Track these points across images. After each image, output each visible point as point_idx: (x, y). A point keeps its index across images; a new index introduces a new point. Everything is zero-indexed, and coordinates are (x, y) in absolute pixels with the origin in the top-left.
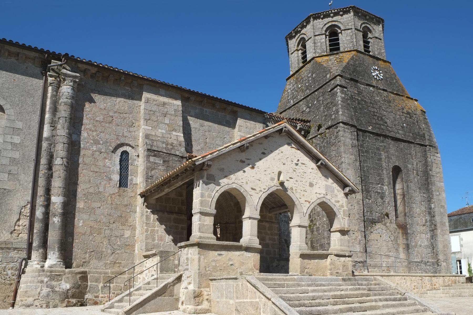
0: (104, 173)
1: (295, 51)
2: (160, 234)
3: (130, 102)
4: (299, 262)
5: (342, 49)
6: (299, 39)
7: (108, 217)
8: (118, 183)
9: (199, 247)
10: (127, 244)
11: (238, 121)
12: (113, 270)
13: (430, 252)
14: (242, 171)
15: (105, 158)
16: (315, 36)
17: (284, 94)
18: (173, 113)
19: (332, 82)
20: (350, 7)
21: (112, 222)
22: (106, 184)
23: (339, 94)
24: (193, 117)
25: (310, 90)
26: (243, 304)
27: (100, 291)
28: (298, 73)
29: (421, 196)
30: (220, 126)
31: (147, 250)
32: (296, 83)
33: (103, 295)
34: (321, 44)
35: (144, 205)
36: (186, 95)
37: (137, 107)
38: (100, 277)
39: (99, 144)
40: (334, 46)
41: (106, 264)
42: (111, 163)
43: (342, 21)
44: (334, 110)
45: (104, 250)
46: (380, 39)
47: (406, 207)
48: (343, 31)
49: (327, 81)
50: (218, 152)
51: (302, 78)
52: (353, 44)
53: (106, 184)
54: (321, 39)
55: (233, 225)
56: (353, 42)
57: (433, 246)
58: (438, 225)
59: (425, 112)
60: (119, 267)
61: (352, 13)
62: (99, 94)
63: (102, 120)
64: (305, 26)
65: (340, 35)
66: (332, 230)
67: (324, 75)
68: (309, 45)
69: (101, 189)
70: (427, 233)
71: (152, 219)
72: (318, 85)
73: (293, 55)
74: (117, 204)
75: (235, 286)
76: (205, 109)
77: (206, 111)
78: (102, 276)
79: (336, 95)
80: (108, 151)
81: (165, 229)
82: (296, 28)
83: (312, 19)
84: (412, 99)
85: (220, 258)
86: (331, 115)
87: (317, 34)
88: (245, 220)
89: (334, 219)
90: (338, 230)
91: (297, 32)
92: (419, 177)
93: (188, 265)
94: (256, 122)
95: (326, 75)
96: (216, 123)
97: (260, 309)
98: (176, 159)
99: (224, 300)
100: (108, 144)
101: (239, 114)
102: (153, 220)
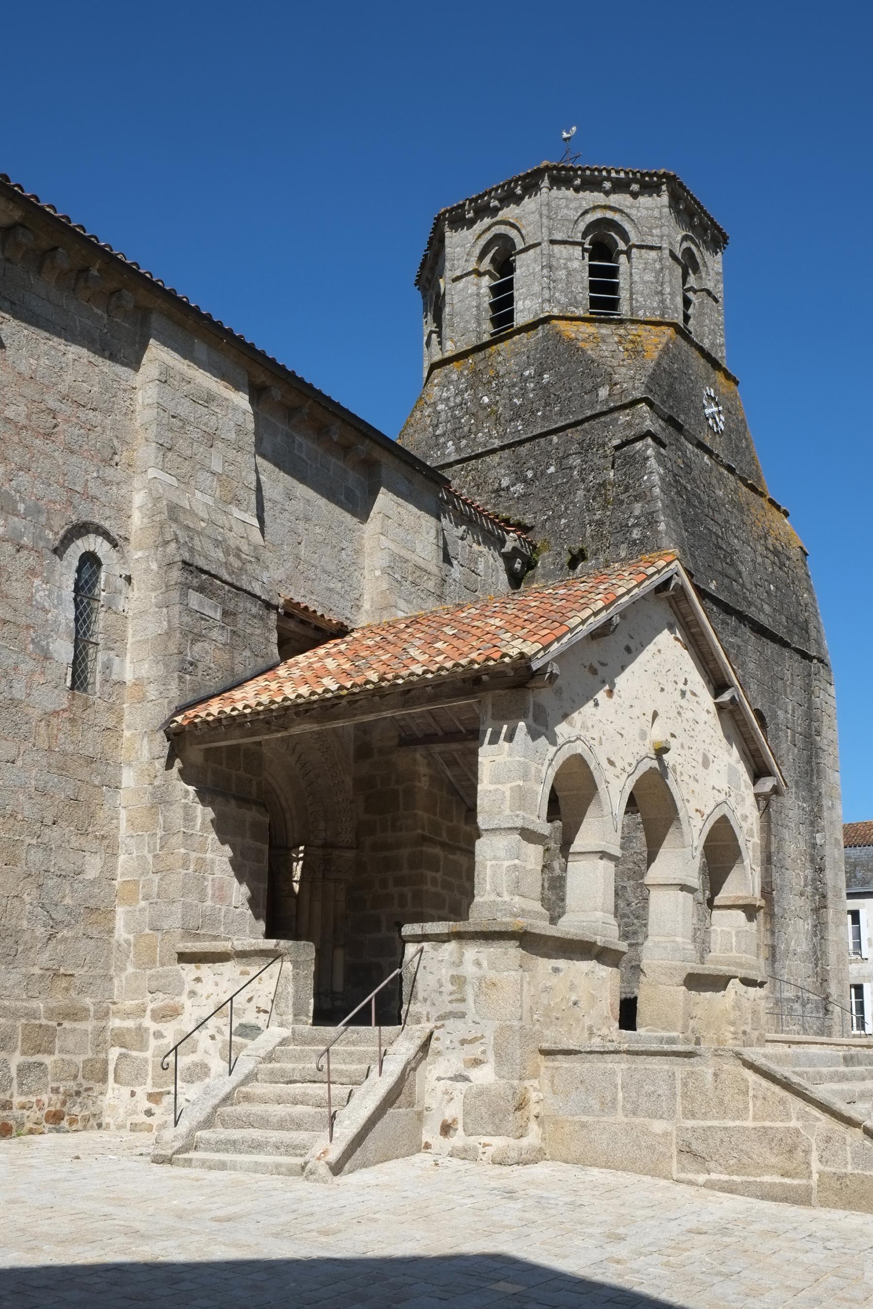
0: (28, 627)
1: (468, 274)
2: (218, 875)
3: (107, 366)
4: (681, 997)
5: (624, 309)
6: (488, 236)
7: (39, 799)
8: (70, 670)
9: (522, 946)
10: (92, 904)
11: (380, 496)
12: (52, 1004)
13: (810, 973)
14: (591, 703)
15: (32, 572)
16: (553, 242)
17: (418, 415)
18: (232, 436)
19: (623, 418)
20: (665, 175)
21: (48, 821)
22: (33, 672)
23: (652, 463)
24: (269, 460)
25: (527, 424)
26: (720, 1135)
27: (15, 1082)
28: (481, 355)
29: (799, 806)
30: (332, 506)
31: (190, 933)
32: (471, 386)
33: (23, 1099)
34: (569, 274)
35: (169, 766)
36: (262, 378)
37: (125, 391)
38: (14, 1028)
39: (15, 513)
40: (604, 296)
41: (29, 977)
42: (51, 592)
43: (633, 212)
44: (637, 512)
45: (25, 924)
46: (716, 301)
47: (773, 837)
48: (634, 250)
49: (599, 408)
50: (569, 636)
51: (497, 376)
52: (663, 301)
53: (33, 672)
54: (570, 259)
55: (350, 854)
56: (661, 293)
57: (818, 955)
58: (830, 895)
59: (806, 554)
60: (67, 990)
61: (665, 199)
62: (16, 316)
63: (24, 422)
64: (518, 200)
65: (623, 258)
66: (717, 901)
67: (589, 386)
68: (525, 267)
69: (19, 692)
70: (807, 918)
71: (199, 821)
72: (560, 413)
73: (461, 284)
74: (64, 753)
75: (679, 1076)
76: (298, 438)
77: (300, 445)
78: (18, 1024)
79: (644, 465)
80: (42, 544)
81: (232, 861)
82: (481, 197)
83: (546, 183)
84: (778, 508)
85: (554, 981)
86: (628, 529)
87: (558, 236)
88: (577, 858)
89: (731, 868)
90: (741, 902)
91: (483, 211)
92: (796, 750)
93: (463, 1000)
94: (421, 509)
95: (596, 388)
96: (323, 495)
97: (807, 1152)
98: (254, 610)
99: (620, 1117)
100: (43, 519)
101: (384, 473)
102: (203, 823)
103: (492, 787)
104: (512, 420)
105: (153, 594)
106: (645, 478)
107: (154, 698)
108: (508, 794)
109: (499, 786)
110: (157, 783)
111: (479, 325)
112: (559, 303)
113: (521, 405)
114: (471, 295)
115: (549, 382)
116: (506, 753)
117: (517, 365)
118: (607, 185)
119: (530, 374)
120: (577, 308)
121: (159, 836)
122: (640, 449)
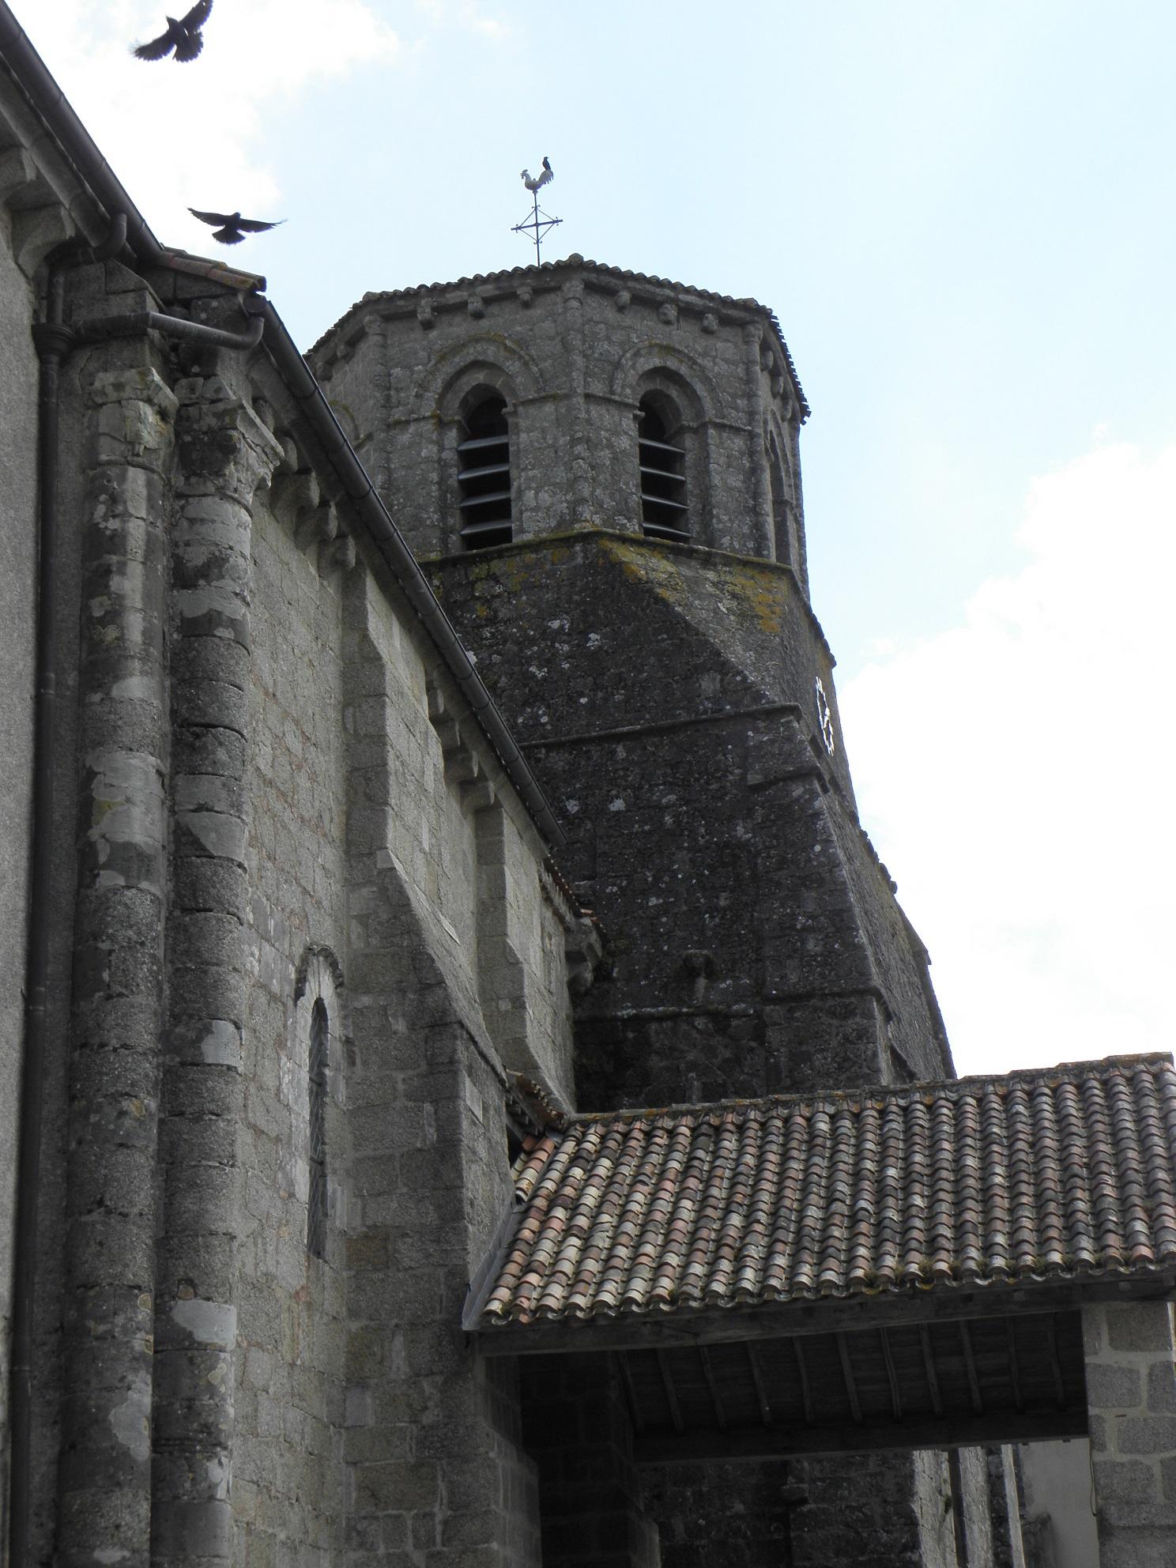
34: (615, 459)
65: (689, 441)
68: (530, 433)
103: (1125, 1458)
104: (526, 703)
105: (400, 1076)
106: (818, 848)
107: (413, 1264)
108: (1157, 1470)
109: (1139, 1457)
110: (427, 1419)
111: (443, 518)
112: (601, 506)
113: (544, 679)
114: (427, 460)
115: (600, 648)
116: (1144, 1404)
117: (533, 606)
118: (625, 296)
119: (562, 627)
120: (629, 519)
121: (439, 1518)
122: (800, 797)
